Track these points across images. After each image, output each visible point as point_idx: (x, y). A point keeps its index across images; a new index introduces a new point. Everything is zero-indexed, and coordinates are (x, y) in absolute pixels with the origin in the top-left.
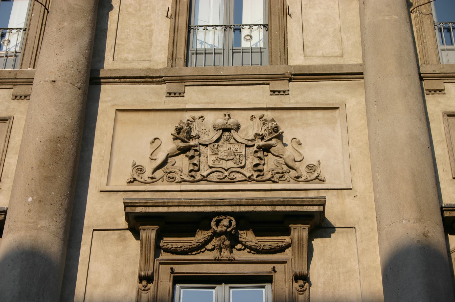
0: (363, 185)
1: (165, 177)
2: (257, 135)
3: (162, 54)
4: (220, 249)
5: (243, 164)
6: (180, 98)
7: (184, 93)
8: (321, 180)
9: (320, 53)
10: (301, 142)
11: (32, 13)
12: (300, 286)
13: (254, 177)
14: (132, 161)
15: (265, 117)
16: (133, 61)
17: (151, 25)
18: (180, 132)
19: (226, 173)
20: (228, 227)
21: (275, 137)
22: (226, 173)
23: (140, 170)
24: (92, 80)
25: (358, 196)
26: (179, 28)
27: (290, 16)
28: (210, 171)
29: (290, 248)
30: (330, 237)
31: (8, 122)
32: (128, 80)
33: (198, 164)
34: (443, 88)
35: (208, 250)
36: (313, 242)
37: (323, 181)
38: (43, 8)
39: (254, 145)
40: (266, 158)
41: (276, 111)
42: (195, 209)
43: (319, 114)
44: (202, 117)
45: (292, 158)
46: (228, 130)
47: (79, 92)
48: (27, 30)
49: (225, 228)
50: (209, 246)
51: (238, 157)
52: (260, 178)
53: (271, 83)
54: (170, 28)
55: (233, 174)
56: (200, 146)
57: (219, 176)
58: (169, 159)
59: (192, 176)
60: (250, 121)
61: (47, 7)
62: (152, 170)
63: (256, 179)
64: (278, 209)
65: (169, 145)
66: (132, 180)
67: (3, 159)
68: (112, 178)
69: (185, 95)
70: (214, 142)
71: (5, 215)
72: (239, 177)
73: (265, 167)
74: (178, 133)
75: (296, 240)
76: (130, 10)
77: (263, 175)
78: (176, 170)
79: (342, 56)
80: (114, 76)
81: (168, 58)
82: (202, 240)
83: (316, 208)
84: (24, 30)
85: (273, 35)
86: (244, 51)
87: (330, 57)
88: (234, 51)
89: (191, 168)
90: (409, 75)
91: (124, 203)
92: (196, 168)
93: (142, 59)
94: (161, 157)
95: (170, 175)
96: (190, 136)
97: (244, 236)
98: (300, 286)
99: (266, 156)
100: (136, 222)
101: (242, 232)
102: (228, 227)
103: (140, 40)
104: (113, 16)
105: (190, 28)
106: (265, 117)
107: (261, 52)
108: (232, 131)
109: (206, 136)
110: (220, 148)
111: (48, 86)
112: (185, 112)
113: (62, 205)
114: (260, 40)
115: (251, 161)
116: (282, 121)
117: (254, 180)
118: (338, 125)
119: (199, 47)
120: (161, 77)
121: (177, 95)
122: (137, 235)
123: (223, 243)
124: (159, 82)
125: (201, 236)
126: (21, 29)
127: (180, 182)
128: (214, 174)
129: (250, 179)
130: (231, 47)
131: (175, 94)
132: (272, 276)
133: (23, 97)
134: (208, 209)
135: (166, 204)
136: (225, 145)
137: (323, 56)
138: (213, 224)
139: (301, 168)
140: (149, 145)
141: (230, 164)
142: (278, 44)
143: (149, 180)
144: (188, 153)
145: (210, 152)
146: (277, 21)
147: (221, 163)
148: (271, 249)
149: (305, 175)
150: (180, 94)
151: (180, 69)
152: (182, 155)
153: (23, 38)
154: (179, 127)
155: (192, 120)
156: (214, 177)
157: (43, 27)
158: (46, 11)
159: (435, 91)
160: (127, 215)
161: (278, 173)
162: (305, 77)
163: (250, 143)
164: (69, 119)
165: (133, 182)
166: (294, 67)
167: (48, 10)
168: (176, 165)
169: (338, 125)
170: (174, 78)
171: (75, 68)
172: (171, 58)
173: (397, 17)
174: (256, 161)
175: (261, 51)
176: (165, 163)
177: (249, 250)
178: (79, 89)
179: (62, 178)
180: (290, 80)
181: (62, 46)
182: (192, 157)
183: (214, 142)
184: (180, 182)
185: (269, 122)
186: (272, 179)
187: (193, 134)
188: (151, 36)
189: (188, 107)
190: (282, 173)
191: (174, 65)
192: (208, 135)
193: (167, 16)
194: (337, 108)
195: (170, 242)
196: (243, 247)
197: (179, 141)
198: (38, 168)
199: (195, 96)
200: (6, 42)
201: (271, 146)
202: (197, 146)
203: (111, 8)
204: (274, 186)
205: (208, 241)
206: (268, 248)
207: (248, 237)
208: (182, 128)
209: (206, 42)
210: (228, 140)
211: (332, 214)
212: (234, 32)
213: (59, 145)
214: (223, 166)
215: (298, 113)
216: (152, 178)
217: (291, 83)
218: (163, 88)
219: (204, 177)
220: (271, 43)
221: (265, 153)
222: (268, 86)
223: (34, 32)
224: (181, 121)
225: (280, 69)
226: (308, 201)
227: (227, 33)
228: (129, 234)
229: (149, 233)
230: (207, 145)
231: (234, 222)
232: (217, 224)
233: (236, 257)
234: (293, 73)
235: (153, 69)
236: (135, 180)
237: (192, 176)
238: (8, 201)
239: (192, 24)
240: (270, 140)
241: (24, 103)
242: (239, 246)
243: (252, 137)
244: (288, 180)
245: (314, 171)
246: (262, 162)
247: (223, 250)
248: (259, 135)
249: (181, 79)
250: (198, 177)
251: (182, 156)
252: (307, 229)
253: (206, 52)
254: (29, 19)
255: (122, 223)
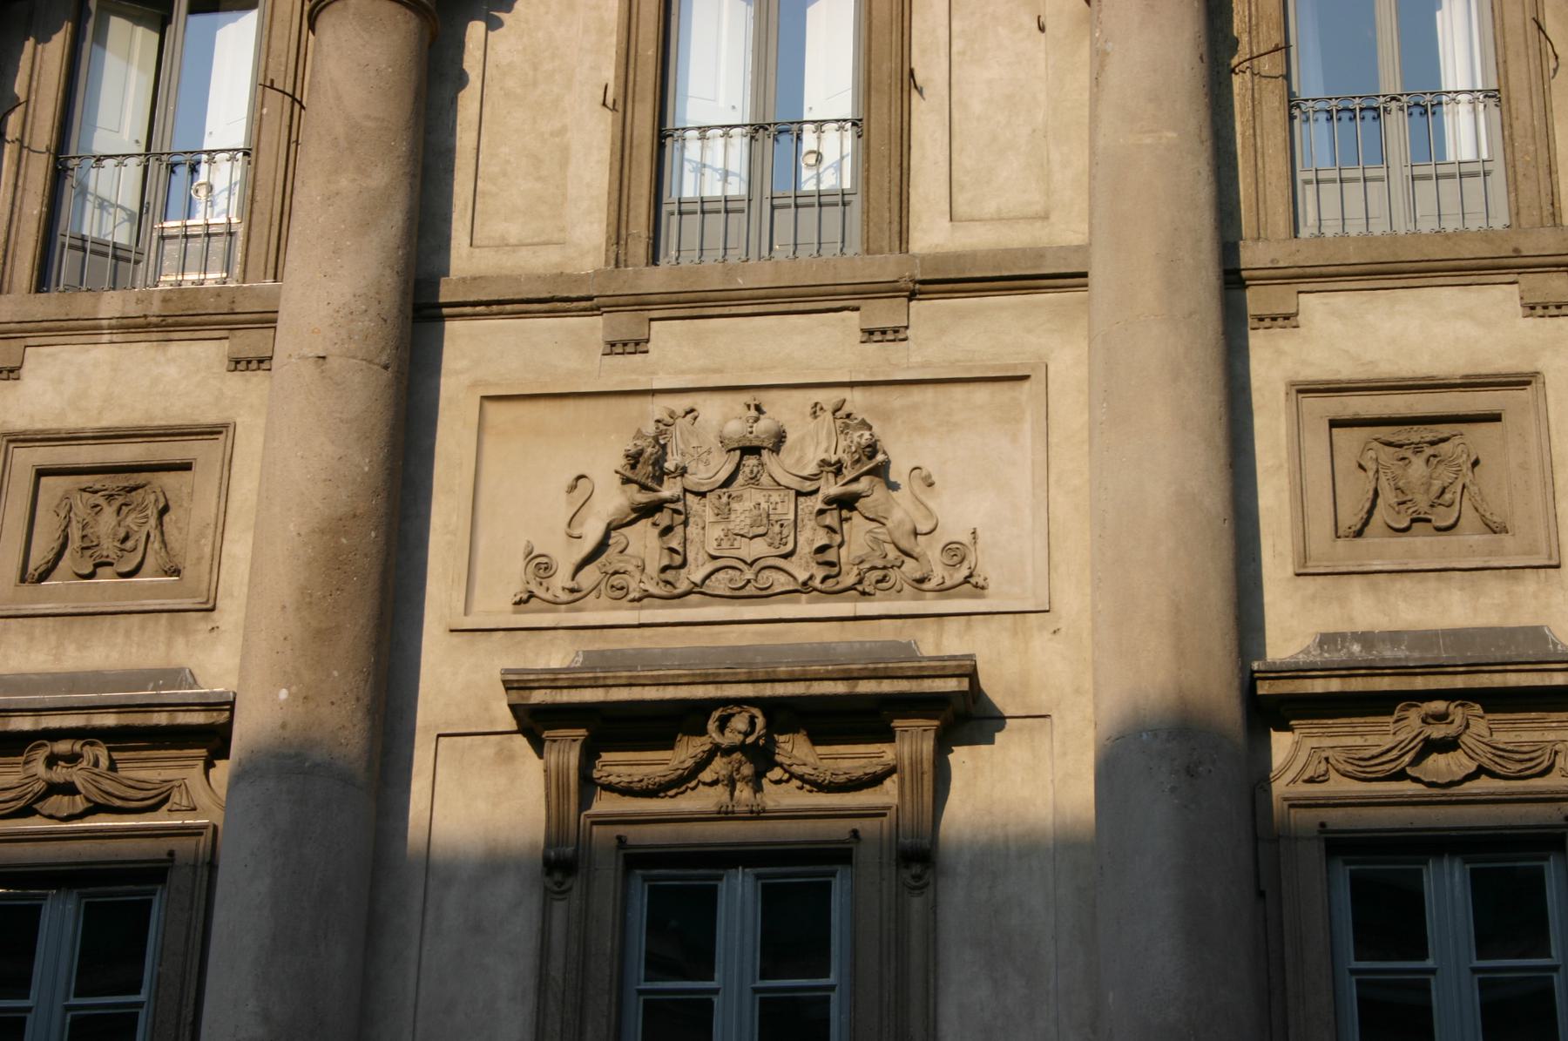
0: (1073, 601)
1: (602, 586)
2: (824, 463)
3: (591, 223)
4: (732, 784)
5: (790, 547)
6: (638, 357)
7: (648, 341)
8: (976, 586)
9: (990, 207)
10: (934, 478)
11: (262, 106)
12: (914, 877)
13: (817, 583)
14: (524, 543)
15: (847, 409)
16: (521, 245)
17: (563, 131)
18: (637, 462)
19: (749, 574)
20: (746, 735)
21: (868, 473)
22: (749, 574)
23: (542, 567)
24: (420, 309)
25: (1063, 630)
26: (635, 142)
27: (920, 92)
28: (709, 567)
29: (895, 777)
30: (991, 741)
31: (221, 437)
32: (509, 308)
33: (680, 549)
34: (1293, 310)
35: (705, 784)
36: (950, 757)
37: (983, 588)
38: (288, 100)
39: (816, 491)
40: (845, 526)
41: (875, 389)
42: (670, 693)
43: (982, 393)
44: (692, 411)
45: (909, 527)
46: (754, 450)
47: (387, 375)
48: (253, 154)
49: (741, 737)
50: (707, 776)
51: (777, 528)
52: (831, 582)
53: (866, 305)
54: (613, 143)
55: (766, 573)
56: (689, 497)
57: (731, 580)
58: (613, 534)
59: (667, 582)
60: (810, 419)
61: (298, 96)
62: (570, 569)
63: (820, 586)
64: (866, 687)
65: (612, 499)
66: (525, 596)
67: (218, 545)
68: (478, 592)
69: (650, 346)
70: (721, 487)
71: (232, 711)
72: (781, 582)
73: (843, 551)
74: (633, 467)
75: (907, 762)
76: (510, 83)
77: (838, 574)
78: (630, 568)
79: (1045, 217)
80: (472, 298)
81: (609, 238)
82: (689, 763)
83: (951, 685)
84: (246, 154)
85: (872, 157)
86: (799, 202)
87: (1017, 219)
88: (776, 202)
89: (665, 562)
90: (1190, 315)
91: (504, 682)
92: (678, 560)
93: (544, 238)
94: (592, 532)
95: (616, 580)
96: (661, 468)
97: (788, 747)
98: (914, 877)
99: (848, 519)
100: (536, 723)
101: (782, 738)
102: (746, 735)
103: (539, 179)
104: (467, 103)
105: (662, 135)
106: (847, 409)
107: (844, 204)
108: (765, 453)
109: (701, 466)
110: (734, 505)
111: (309, 370)
112: (649, 399)
113: (358, 699)
114: (842, 158)
115: (811, 536)
116: (887, 416)
117: (815, 589)
118: (1027, 426)
119: (689, 192)
120: (590, 298)
121: (630, 348)
122: (538, 746)
123: (738, 770)
124: (585, 310)
125: (687, 751)
126: (238, 150)
127: (640, 600)
128: (721, 575)
129: (806, 587)
130: (767, 193)
131: (625, 345)
132: (850, 850)
133: (254, 365)
134: (700, 692)
135: (601, 682)
136: (746, 494)
137: (999, 219)
138: (712, 726)
139: (929, 553)
140: (564, 495)
141: (759, 548)
142: (886, 185)
143: (565, 597)
144: (657, 516)
145: (709, 515)
146: (885, 110)
147: (736, 544)
148: (850, 780)
149: (939, 574)
150: (637, 344)
151: (635, 272)
152: (643, 522)
153: (245, 174)
154: (633, 450)
155: (668, 420)
156: (720, 584)
157: (293, 146)
158: (297, 107)
159: (1274, 319)
160: (512, 707)
161: (874, 568)
162: (950, 286)
163: (808, 486)
164: (363, 461)
165: (526, 601)
166: (923, 258)
167: (300, 103)
168: (628, 551)
169: (1027, 426)
170: (622, 300)
171: (373, 312)
172: (614, 240)
173: (1175, 135)
174: (822, 539)
175: (843, 200)
176: (601, 547)
177: (799, 783)
178: (386, 367)
179: (355, 626)
180: (912, 296)
181: (336, 252)
182: (667, 531)
183: (721, 487)
184: (640, 600)
185: (855, 430)
186: (860, 588)
187: (669, 465)
188: (564, 163)
189: (656, 386)
190: (885, 568)
191: (622, 258)
192: (707, 463)
193: (604, 104)
194: (1025, 378)
195: (618, 765)
196: (786, 776)
197: (635, 487)
198: (298, 609)
199: (678, 351)
200: (203, 192)
201: (857, 497)
202: (678, 500)
203: (461, 80)
204: (865, 608)
205: (702, 764)
206: (842, 779)
207: (796, 749)
208: (640, 453)
209: (708, 162)
210: (754, 480)
211: (994, 688)
212: (776, 139)
213: (344, 541)
214: (743, 553)
215: (929, 393)
216: (572, 591)
217: (913, 303)
218: (594, 328)
219: (696, 585)
220: (868, 183)
221: (845, 513)
222: (856, 314)
223: (270, 161)
224: (639, 431)
225: (886, 268)
226: (934, 668)
227: (757, 146)
228: (521, 742)
229: (567, 751)
230: (703, 495)
231: (760, 722)
232: (722, 728)
233: (770, 804)
234: (919, 277)
235: (570, 276)
236: (531, 595)
237: (667, 582)
238: (237, 660)
239: (669, 126)
240: (856, 479)
241: (257, 381)
242: (777, 773)
243: (812, 469)
244: (898, 587)
245: (961, 562)
246: (838, 539)
247: (739, 785)
248: (830, 464)
249: (640, 303)
250: (683, 586)
251: (644, 524)
252: (932, 734)
253: (704, 207)
254: (256, 123)
255: (507, 721)
